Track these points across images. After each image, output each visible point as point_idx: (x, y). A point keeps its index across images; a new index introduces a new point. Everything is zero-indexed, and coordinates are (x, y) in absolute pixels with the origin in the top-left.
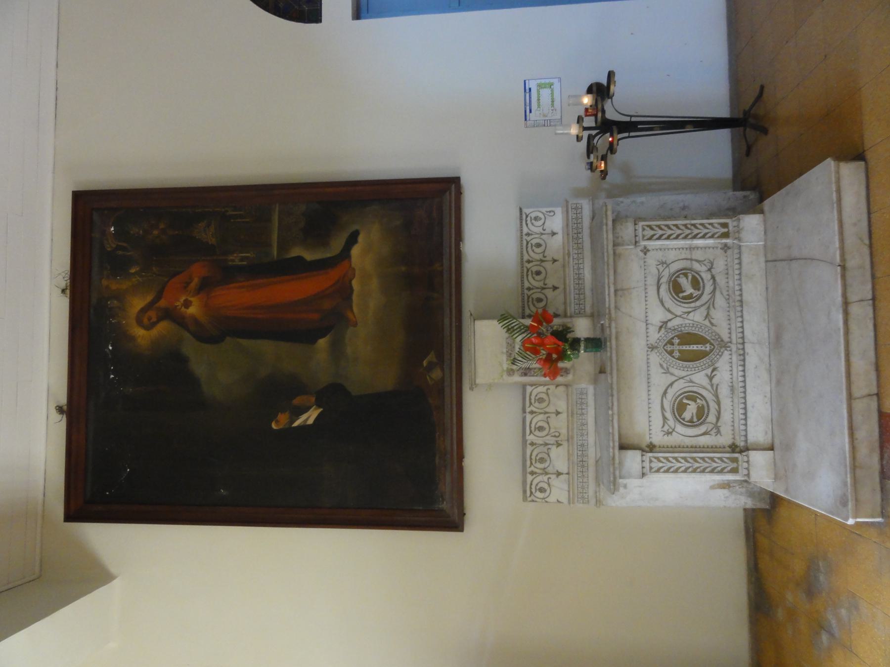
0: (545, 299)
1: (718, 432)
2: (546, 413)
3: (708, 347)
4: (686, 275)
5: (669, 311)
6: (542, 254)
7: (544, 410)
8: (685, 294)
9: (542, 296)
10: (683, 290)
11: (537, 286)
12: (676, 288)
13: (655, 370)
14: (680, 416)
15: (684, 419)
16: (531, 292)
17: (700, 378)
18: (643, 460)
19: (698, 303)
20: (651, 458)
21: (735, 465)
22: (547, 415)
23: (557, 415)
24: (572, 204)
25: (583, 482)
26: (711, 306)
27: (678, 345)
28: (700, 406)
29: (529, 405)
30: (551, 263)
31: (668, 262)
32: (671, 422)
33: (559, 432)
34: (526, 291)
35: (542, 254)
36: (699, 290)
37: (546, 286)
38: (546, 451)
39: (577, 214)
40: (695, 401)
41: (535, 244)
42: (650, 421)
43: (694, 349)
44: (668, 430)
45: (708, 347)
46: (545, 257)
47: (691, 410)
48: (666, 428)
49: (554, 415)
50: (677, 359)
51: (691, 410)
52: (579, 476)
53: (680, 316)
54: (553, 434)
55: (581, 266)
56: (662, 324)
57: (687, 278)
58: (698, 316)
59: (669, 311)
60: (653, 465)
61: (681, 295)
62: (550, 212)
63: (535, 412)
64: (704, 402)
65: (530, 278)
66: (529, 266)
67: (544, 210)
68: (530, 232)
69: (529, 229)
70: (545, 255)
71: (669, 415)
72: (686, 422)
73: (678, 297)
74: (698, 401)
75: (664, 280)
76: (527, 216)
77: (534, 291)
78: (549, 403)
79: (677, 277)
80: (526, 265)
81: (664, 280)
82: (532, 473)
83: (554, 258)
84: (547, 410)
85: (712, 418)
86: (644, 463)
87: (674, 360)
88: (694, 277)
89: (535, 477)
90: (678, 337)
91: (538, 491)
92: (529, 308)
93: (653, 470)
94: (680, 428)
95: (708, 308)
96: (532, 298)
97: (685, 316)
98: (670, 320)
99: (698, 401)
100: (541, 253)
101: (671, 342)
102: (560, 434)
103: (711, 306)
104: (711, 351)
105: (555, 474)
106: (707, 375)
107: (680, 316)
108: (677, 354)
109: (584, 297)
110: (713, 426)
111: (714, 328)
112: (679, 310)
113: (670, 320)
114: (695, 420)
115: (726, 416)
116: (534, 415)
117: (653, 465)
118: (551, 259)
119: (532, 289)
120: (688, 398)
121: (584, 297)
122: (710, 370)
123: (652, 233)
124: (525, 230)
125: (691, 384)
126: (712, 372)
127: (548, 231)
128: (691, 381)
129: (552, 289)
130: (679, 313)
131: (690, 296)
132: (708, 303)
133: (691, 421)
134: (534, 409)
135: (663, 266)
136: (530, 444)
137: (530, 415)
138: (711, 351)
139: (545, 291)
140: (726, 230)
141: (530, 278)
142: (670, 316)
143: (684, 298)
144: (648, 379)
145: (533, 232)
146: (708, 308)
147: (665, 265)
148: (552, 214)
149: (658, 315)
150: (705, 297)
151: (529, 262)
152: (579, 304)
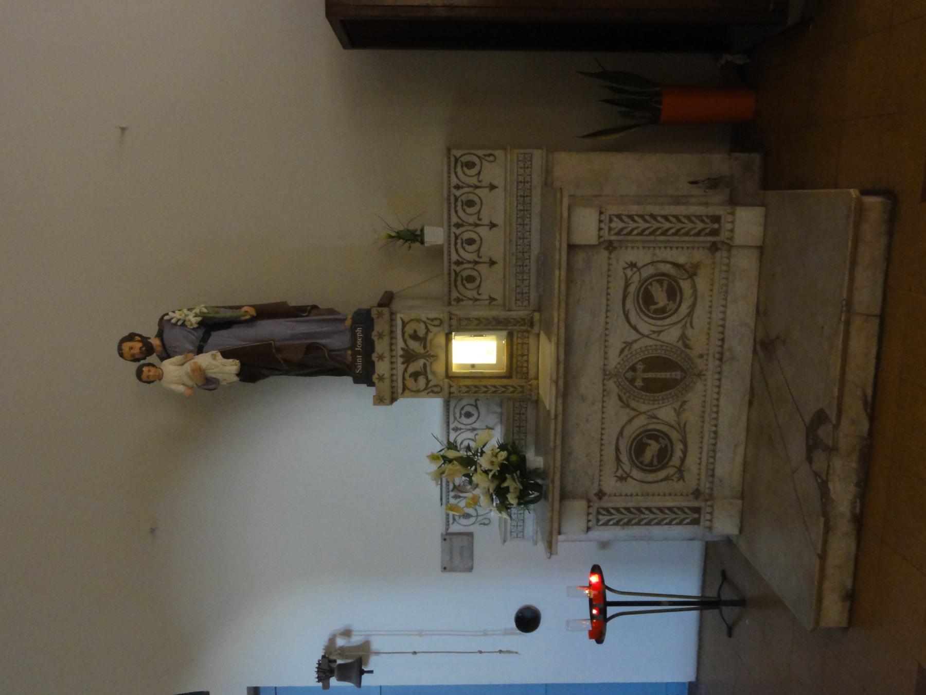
0: (479, 242)
1: (681, 478)
2: (474, 429)
3: (678, 375)
4: (660, 282)
5: (635, 328)
6: (476, 178)
7: (472, 426)
8: (656, 307)
9: (474, 273)
10: (656, 301)
11: (468, 259)
12: (647, 299)
13: (613, 403)
14: (637, 458)
15: (641, 463)
16: (461, 229)
17: (666, 413)
18: (602, 219)
19: (674, 319)
20: (612, 216)
21: (696, 516)
22: (475, 432)
23: (491, 190)
24: (516, 306)
25: (523, 266)
26: (688, 325)
27: (644, 371)
28: (663, 446)
29: (453, 420)
30: (487, 302)
31: (640, 264)
32: (627, 465)
33: (489, 519)
34: (454, 267)
35: (477, 215)
36: (674, 300)
37: (481, 260)
38: (473, 437)
39: (524, 168)
40: (657, 441)
41: (466, 277)
42: (601, 450)
43: (665, 373)
44: (622, 475)
45: (678, 375)
46: (480, 181)
47: (652, 449)
48: (620, 473)
49: (486, 266)
50: (639, 389)
51: (652, 449)
52: (518, 230)
53: (647, 336)
54: (482, 522)
55: (523, 417)
56: (625, 345)
57: (662, 287)
58: (672, 336)
59: (635, 328)
60: (613, 225)
61: (653, 307)
62: (489, 155)
63: (461, 429)
64: (667, 442)
65: (459, 170)
66: (458, 193)
67: (480, 153)
68: (460, 184)
69: (459, 255)
70: (480, 255)
71: (624, 458)
72: (646, 466)
73: (649, 310)
74: (661, 440)
75: (632, 289)
76: (456, 199)
77: (465, 266)
78: (482, 204)
79: (648, 285)
80: (454, 191)
81: (632, 289)
82: (456, 429)
83: (493, 222)
84: (475, 426)
85: (676, 460)
86: (602, 232)
87: (636, 390)
88: (669, 284)
89: (460, 434)
90: (644, 361)
91: (463, 417)
92: (457, 176)
93: (601, 523)
94: (636, 473)
95: (684, 326)
96: (461, 161)
97: (654, 336)
98: (635, 341)
99: (661, 440)
100: (476, 214)
101: (633, 369)
102: (490, 521)
103: (688, 325)
104: (682, 379)
105: (488, 263)
106: (675, 409)
107: (647, 336)
108: (639, 383)
109: (529, 283)
110: (676, 470)
111: (688, 351)
112: (645, 328)
113: (635, 341)
114: (655, 462)
115: (691, 460)
116: (459, 432)
117: (613, 225)
118: (487, 260)
119: (462, 187)
120: (650, 437)
121: (529, 283)
122: (679, 403)
123: (622, 225)
124: (454, 219)
125: (654, 420)
126: (681, 406)
127: (486, 182)
128: (655, 417)
129: (489, 264)
130: (646, 332)
131: (662, 310)
132: (684, 322)
133: (651, 464)
134: (460, 426)
135: (631, 270)
136: (453, 429)
137: (454, 499)
138: (682, 379)
139: (478, 267)
140: (716, 226)
141: (459, 170)
142: (635, 336)
143: (657, 311)
144: (601, 466)
145: (464, 259)
146: (684, 326)
147: (635, 269)
148: (492, 158)
149: (620, 334)
150: (684, 310)
151: (458, 187)
152: (520, 414)
